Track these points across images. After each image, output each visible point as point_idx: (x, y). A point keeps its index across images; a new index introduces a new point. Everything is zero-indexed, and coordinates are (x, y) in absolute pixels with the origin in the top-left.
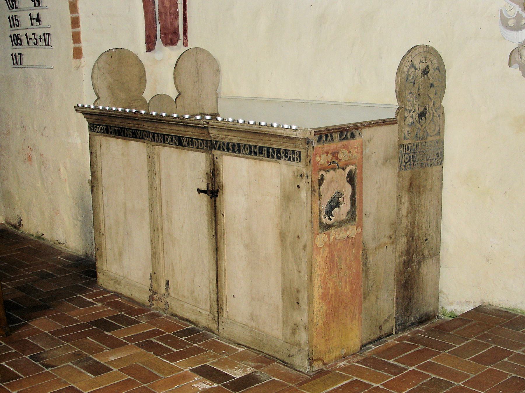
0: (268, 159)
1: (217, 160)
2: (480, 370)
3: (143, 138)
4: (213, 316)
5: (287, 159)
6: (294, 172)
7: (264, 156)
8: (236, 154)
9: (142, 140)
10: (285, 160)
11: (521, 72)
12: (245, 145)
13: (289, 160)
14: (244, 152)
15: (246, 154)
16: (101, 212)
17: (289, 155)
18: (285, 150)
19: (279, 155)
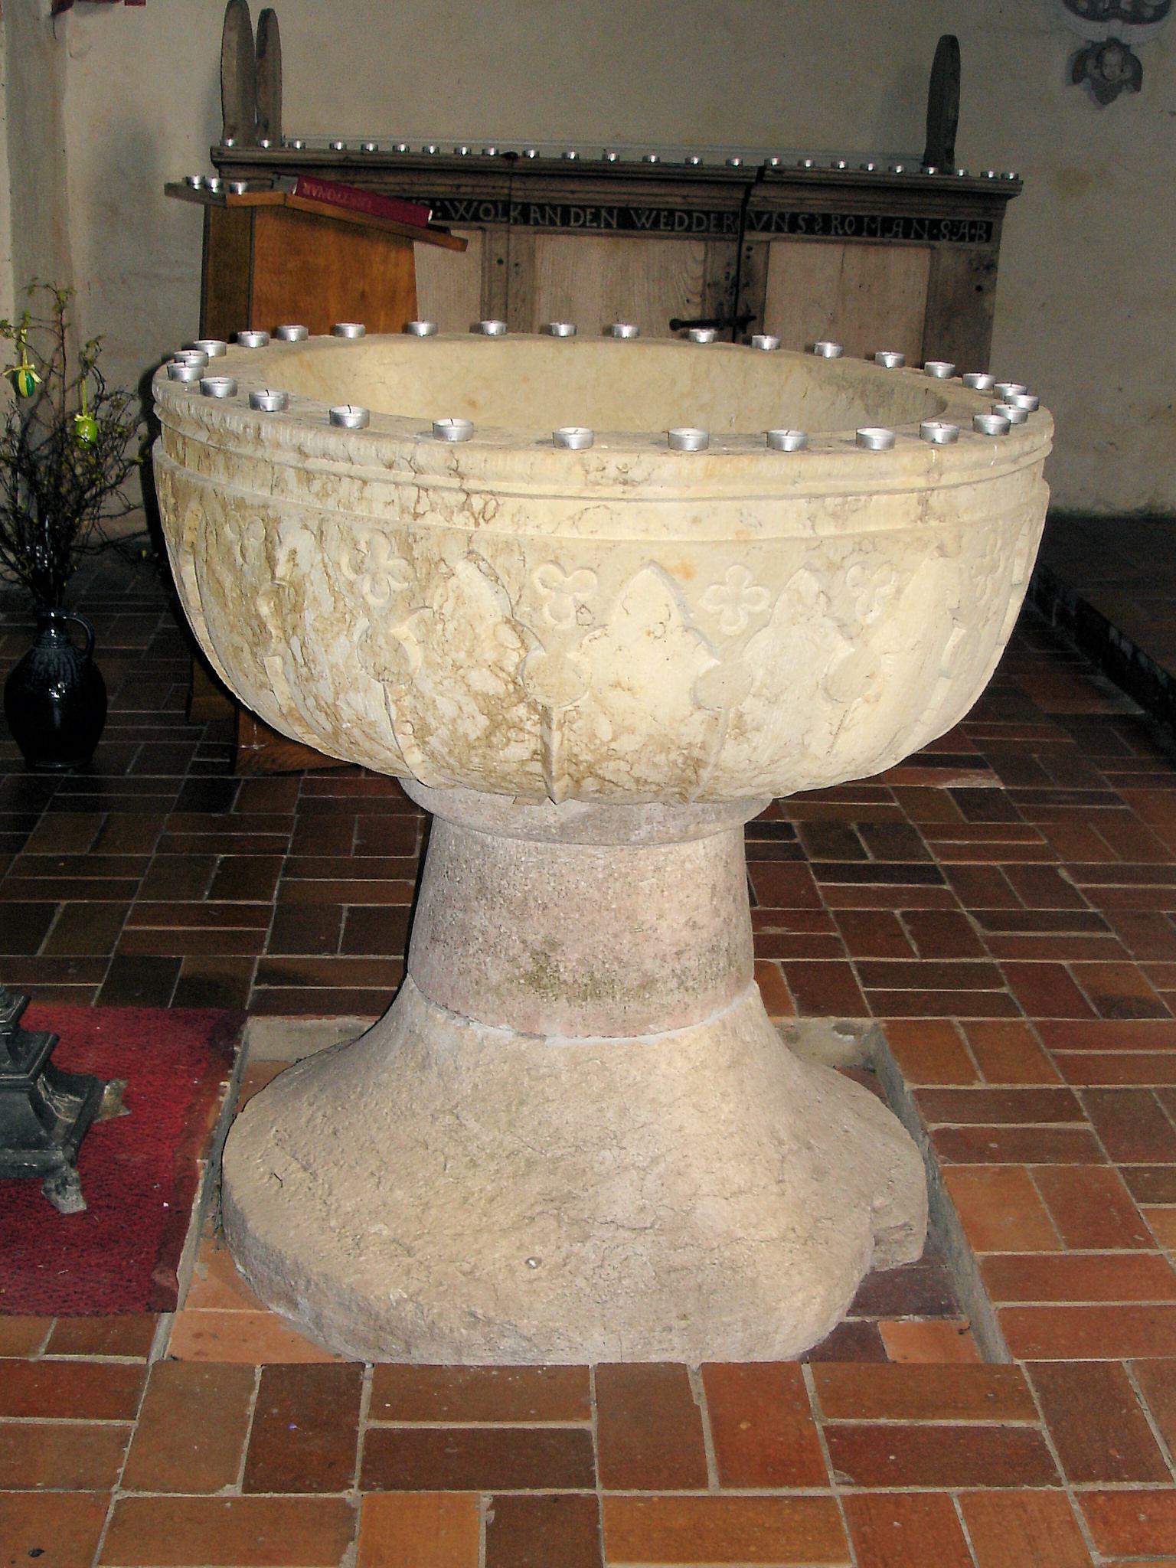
0: (906, 241)
1: (752, 253)
2: (506, 213)
3: (476, 218)
4: (52, 297)
5: (954, 238)
6: (970, 262)
7: (896, 236)
8: (817, 237)
9: (475, 224)
10: (950, 239)
11: (1104, 40)
12: (844, 217)
13: (962, 238)
14: (840, 232)
15: (845, 234)
16: (985, 781)
17: (962, 231)
18: (952, 222)
19: (935, 231)
